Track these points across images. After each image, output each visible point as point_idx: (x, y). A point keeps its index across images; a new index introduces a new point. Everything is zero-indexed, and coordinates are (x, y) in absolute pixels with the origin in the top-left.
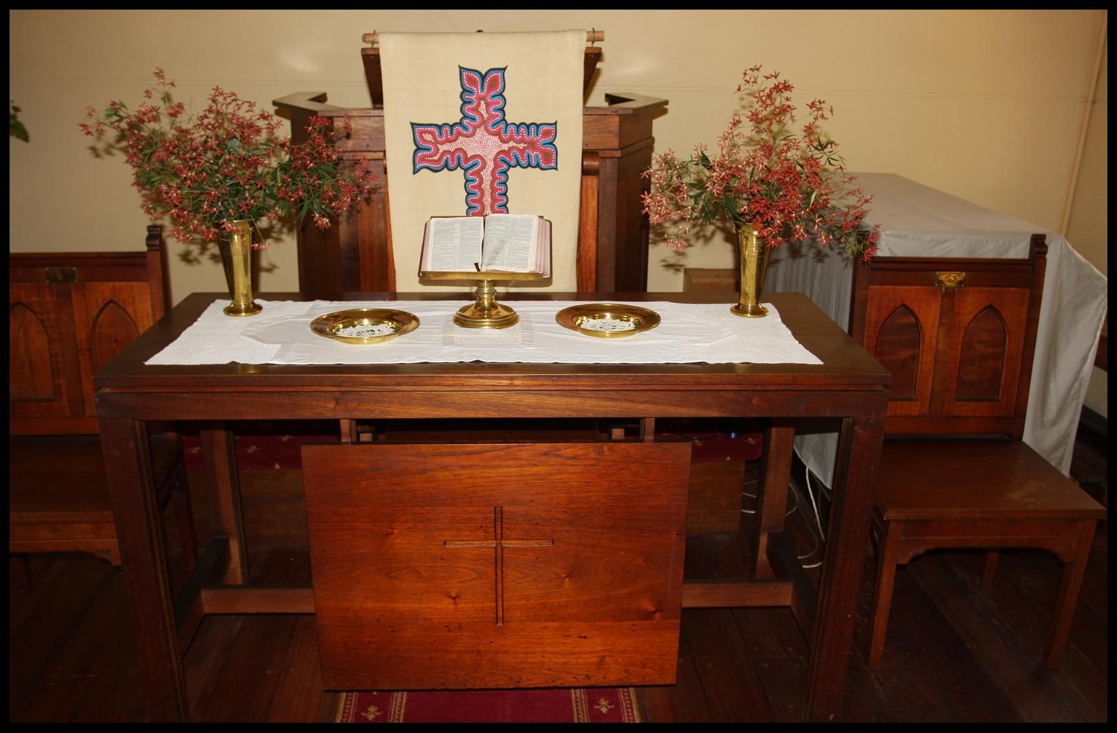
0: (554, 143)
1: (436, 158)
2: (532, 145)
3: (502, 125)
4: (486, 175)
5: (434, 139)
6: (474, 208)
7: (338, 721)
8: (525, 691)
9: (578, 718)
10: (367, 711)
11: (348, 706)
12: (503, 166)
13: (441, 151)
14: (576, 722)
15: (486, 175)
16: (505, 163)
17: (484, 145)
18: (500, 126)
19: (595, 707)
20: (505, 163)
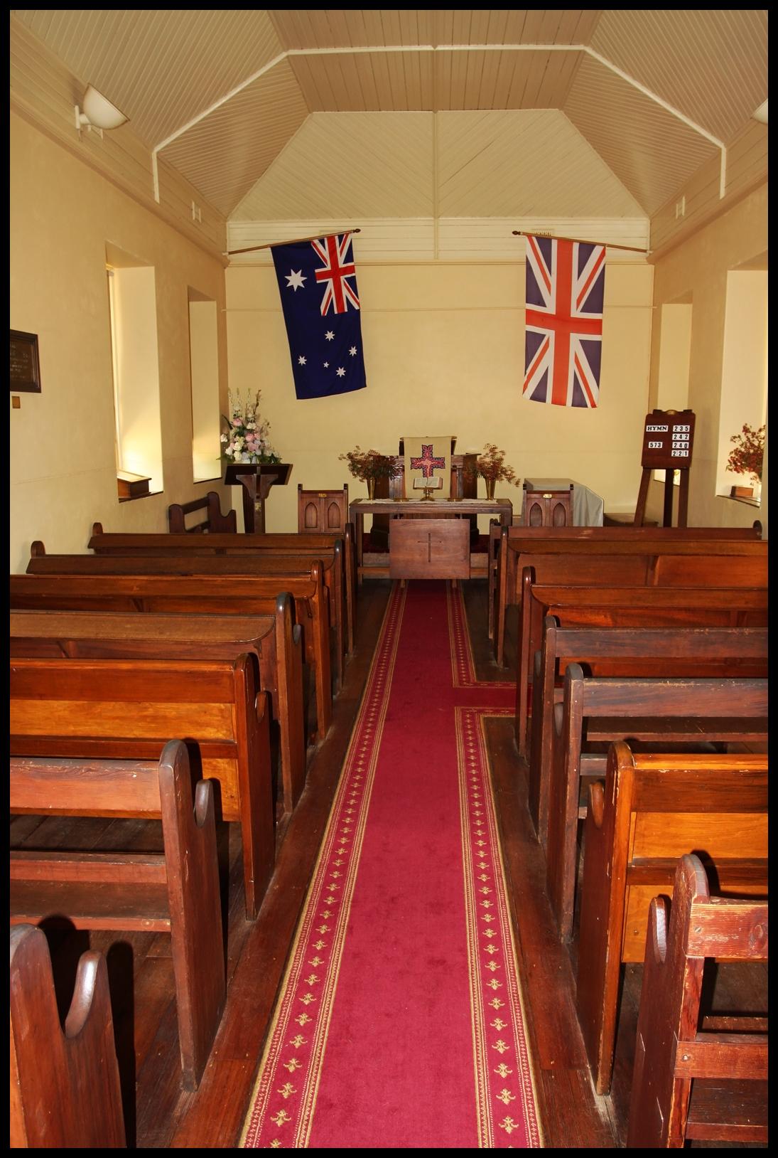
2: (439, 463)
4: (428, 470)
6: (425, 475)
7: (242, 1145)
9: (483, 1144)
10: (276, 1116)
11: (258, 1112)
14: (481, 1147)
15: (428, 470)
16: (432, 467)
17: (427, 463)
18: (431, 458)
19: (497, 1096)
20: (432, 467)
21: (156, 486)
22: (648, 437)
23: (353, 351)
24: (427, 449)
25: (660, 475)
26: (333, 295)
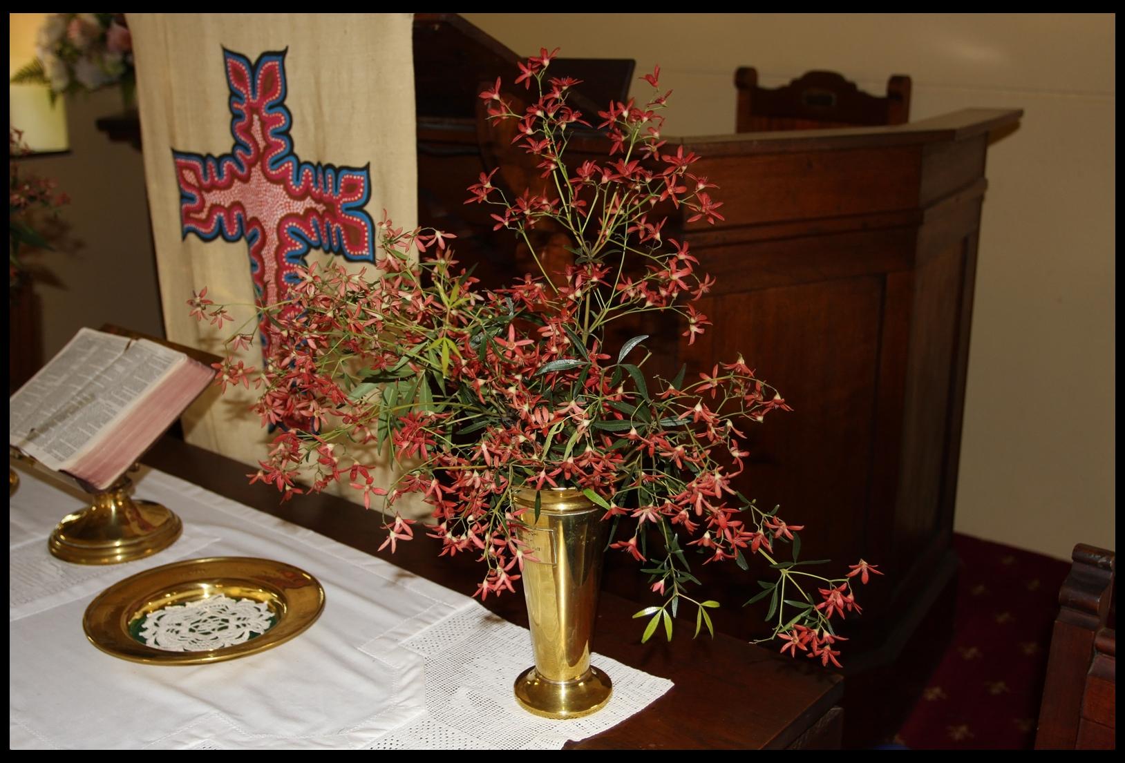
0: (367, 208)
1: (203, 215)
3: (290, 165)
5: (198, 181)
8: (550, 547)
12: (295, 245)
13: (208, 205)
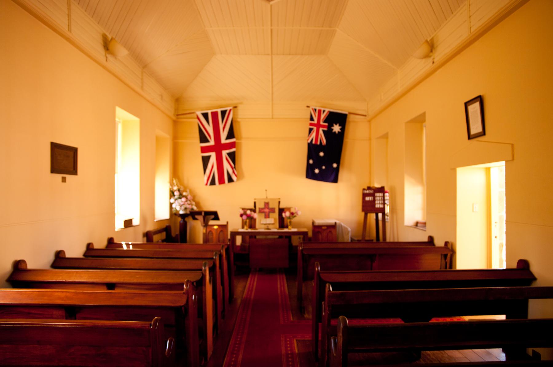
17: (267, 210)
18: (268, 208)
20: (269, 212)
21: (136, 222)
22: (364, 195)
23: (335, 165)
24: (267, 204)
25: (372, 216)
26: (221, 126)
